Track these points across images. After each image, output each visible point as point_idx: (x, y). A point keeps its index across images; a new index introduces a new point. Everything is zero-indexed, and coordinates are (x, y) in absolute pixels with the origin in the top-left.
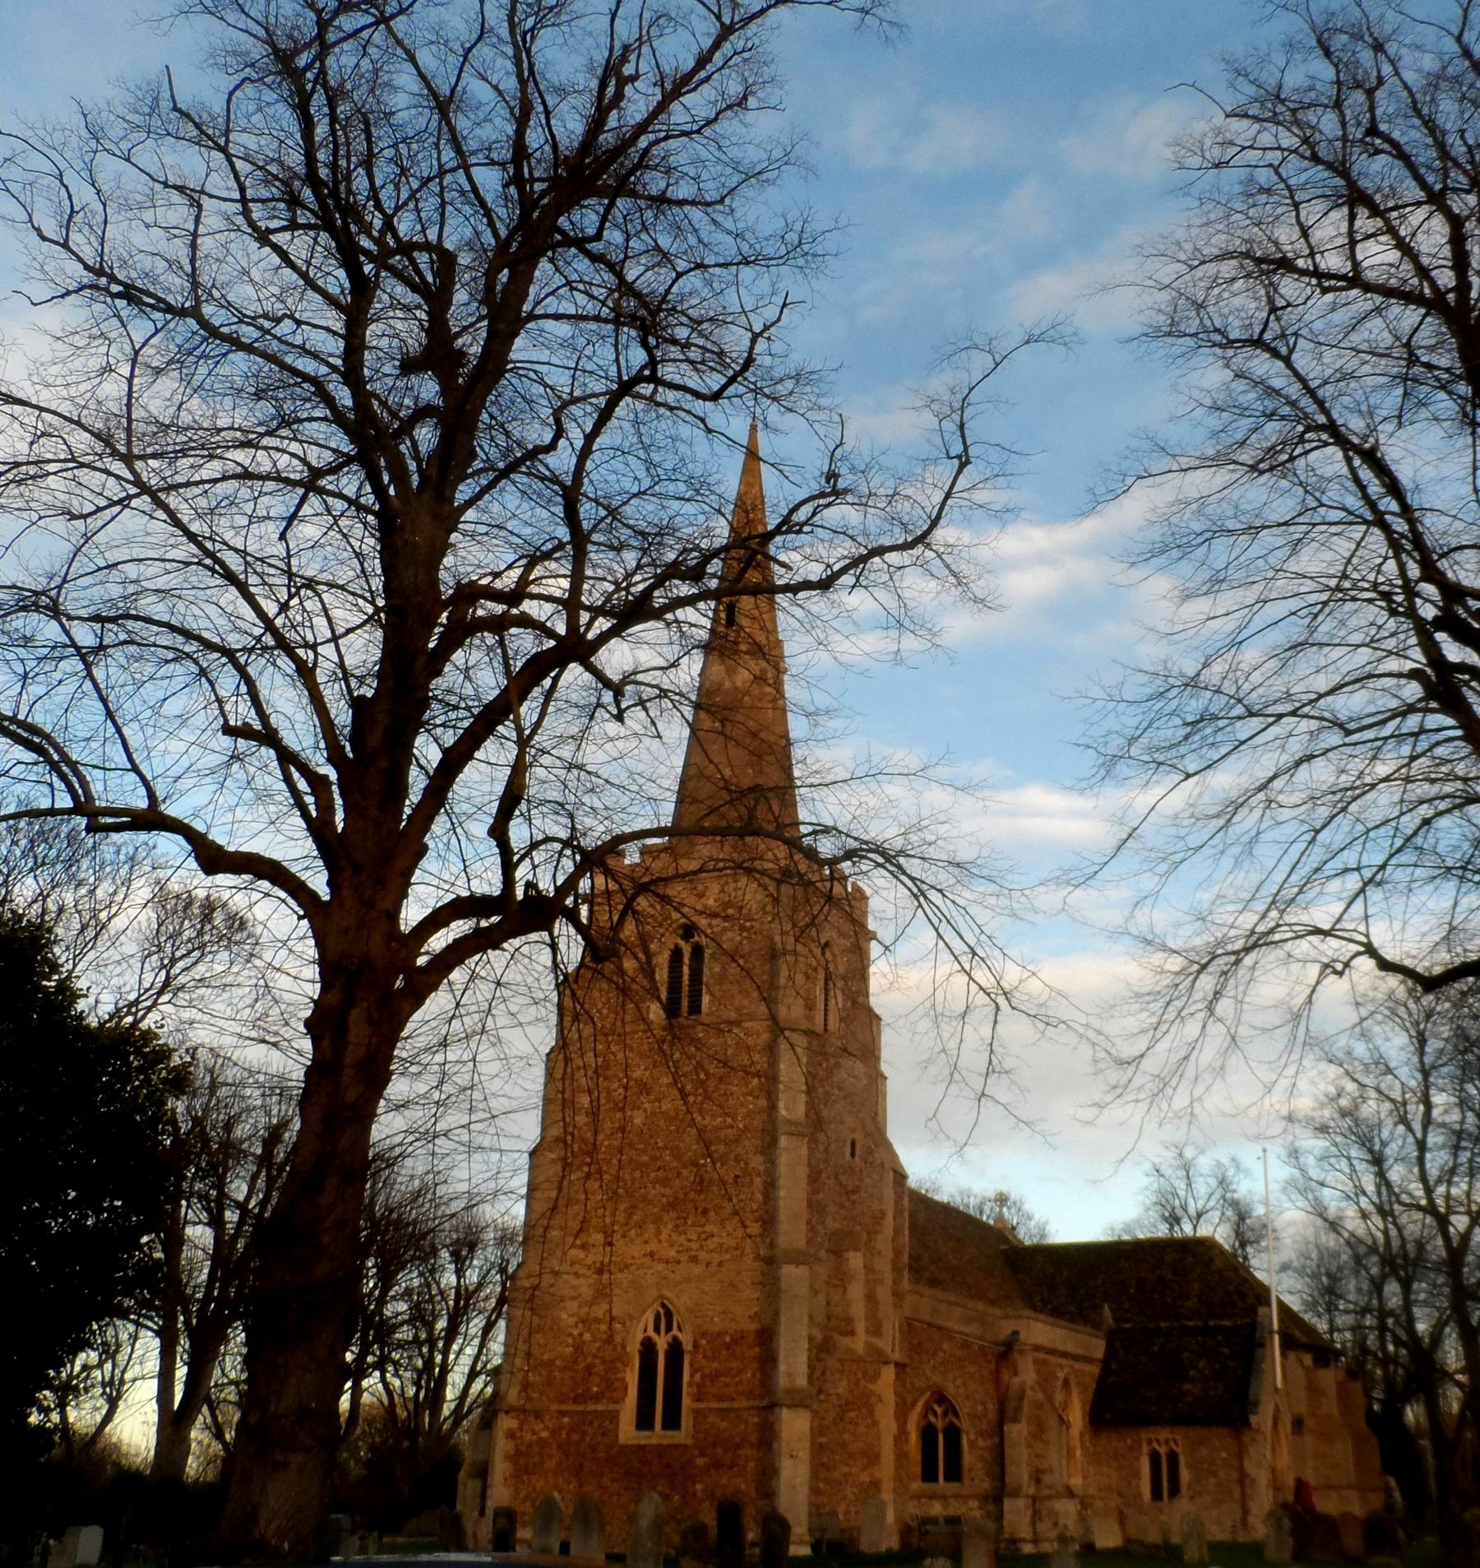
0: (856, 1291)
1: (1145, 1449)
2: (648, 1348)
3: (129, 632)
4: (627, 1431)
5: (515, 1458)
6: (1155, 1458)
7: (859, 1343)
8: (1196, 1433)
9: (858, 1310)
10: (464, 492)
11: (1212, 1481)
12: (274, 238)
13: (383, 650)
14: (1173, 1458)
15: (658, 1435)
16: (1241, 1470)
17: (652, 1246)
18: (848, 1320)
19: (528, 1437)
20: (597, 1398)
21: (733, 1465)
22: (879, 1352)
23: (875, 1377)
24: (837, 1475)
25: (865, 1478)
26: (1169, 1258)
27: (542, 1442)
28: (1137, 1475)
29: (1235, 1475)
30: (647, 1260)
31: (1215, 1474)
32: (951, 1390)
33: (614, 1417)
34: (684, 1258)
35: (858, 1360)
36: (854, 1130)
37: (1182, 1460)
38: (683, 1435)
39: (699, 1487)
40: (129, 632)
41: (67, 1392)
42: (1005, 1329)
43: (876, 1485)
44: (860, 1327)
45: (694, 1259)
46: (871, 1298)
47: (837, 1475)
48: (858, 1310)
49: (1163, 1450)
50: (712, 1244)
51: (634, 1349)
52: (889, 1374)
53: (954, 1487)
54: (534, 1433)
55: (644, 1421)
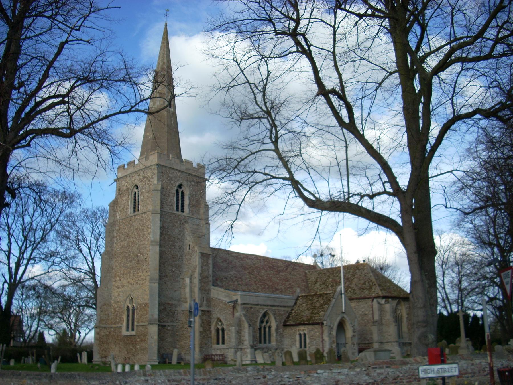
1: (298, 333)
2: (128, 307)
3: (488, 237)
6: (300, 335)
10: (21, 44)
11: (315, 342)
14: (305, 334)
15: (131, 333)
16: (322, 338)
17: (129, 280)
18: (186, 298)
19: (103, 334)
20: (118, 323)
21: (145, 340)
26: (337, 278)
28: (295, 341)
29: (321, 340)
30: (127, 284)
32: (222, 319)
34: (135, 283)
36: (190, 241)
37: (307, 336)
38: (134, 333)
39: (138, 347)
40: (488, 237)
45: (137, 283)
46: (192, 291)
49: (302, 333)
50: (140, 279)
51: (126, 308)
53: (224, 346)
54: (104, 333)
55: (127, 329)
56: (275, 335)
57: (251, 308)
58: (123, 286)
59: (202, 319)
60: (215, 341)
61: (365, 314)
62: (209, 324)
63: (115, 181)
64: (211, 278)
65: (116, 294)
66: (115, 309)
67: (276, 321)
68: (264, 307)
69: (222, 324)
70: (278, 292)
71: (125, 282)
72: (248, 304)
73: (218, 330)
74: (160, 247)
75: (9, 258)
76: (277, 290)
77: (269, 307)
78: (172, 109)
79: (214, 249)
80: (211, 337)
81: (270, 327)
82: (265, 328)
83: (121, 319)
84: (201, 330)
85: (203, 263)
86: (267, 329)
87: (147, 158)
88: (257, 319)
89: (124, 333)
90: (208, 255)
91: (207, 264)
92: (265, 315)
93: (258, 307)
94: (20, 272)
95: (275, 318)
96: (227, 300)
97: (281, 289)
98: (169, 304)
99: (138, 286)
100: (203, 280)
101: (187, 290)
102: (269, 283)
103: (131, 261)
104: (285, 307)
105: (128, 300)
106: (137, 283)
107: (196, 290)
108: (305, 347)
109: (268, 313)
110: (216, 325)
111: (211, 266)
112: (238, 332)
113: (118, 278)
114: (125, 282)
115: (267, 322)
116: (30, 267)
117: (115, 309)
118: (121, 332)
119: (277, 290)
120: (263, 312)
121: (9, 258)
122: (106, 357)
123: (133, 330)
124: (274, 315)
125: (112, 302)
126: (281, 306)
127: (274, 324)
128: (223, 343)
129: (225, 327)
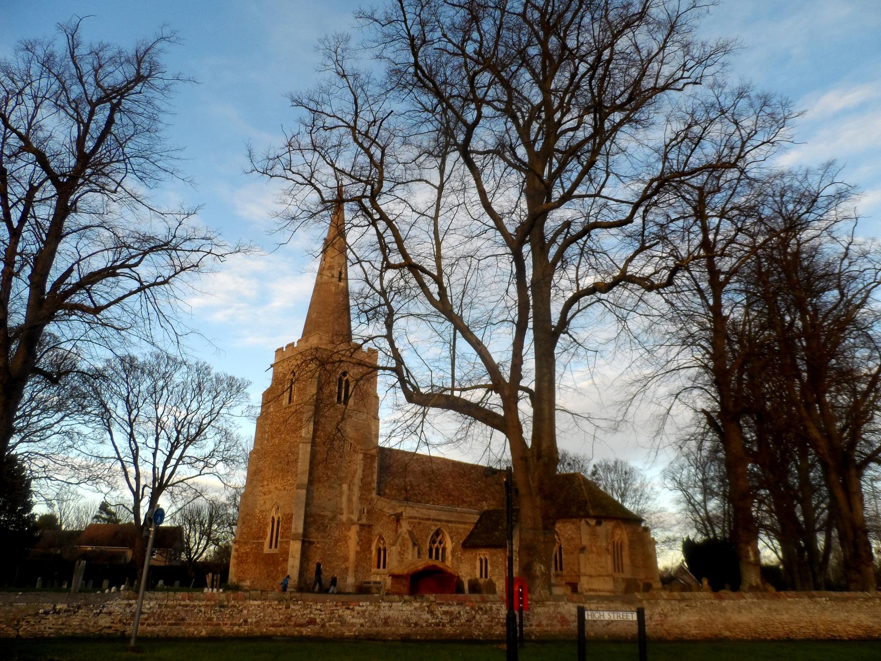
0: (344, 498)
2: (273, 518)
4: (266, 550)
5: (521, 548)
7: (344, 518)
8: (493, 551)
9: (344, 505)
12: (363, 263)
13: (517, 408)
15: (274, 550)
18: (342, 509)
22: (352, 520)
23: (349, 529)
24: (333, 565)
25: (343, 566)
27: (247, 553)
28: (475, 568)
31: (498, 567)
33: (263, 544)
35: (343, 524)
38: (276, 551)
41: (766, 539)
42: (399, 510)
43: (347, 568)
44: (345, 511)
46: (350, 500)
47: (333, 565)
48: (344, 505)
52: (355, 529)
55: (271, 547)
56: (450, 558)
57: (419, 523)
58: (270, 492)
59: (359, 536)
60: (376, 564)
61: (572, 538)
62: (370, 541)
63: (272, 366)
64: (375, 485)
65: (262, 502)
66: (259, 520)
67: (452, 542)
68: (438, 523)
69: (384, 542)
70: (465, 505)
71: (272, 487)
72: (415, 518)
73: (379, 551)
74: (312, 446)
75: (154, 455)
76: (464, 502)
77: (444, 523)
78: (342, 284)
79: (382, 450)
80: (370, 559)
81: (444, 549)
82: (437, 550)
83: (265, 533)
84: (358, 549)
85: (365, 466)
86: (440, 551)
87: (307, 341)
88: (427, 537)
89: (266, 550)
90: (373, 457)
91: (371, 467)
92: (437, 533)
93: (428, 522)
94: (168, 472)
95: (451, 538)
96: (391, 512)
97: (470, 501)
98: (320, 516)
99: (285, 492)
100: (365, 486)
101: (344, 498)
102: (456, 493)
103: (280, 462)
104: (465, 523)
105: (274, 509)
106: (285, 489)
107: (355, 499)
108: (561, 569)
109: (443, 532)
110: (377, 544)
111: (376, 470)
112: (400, 553)
113: (266, 483)
114: (272, 487)
115: (440, 543)
116: (179, 468)
117: (259, 520)
118: (262, 550)
119: (464, 502)
120: (434, 529)
121: (154, 455)
122: (243, 581)
123: (276, 547)
124: (450, 533)
125: (257, 511)
126: (460, 523)
127: (449, 545)
128: (384, 567)
129: (387, 546)
